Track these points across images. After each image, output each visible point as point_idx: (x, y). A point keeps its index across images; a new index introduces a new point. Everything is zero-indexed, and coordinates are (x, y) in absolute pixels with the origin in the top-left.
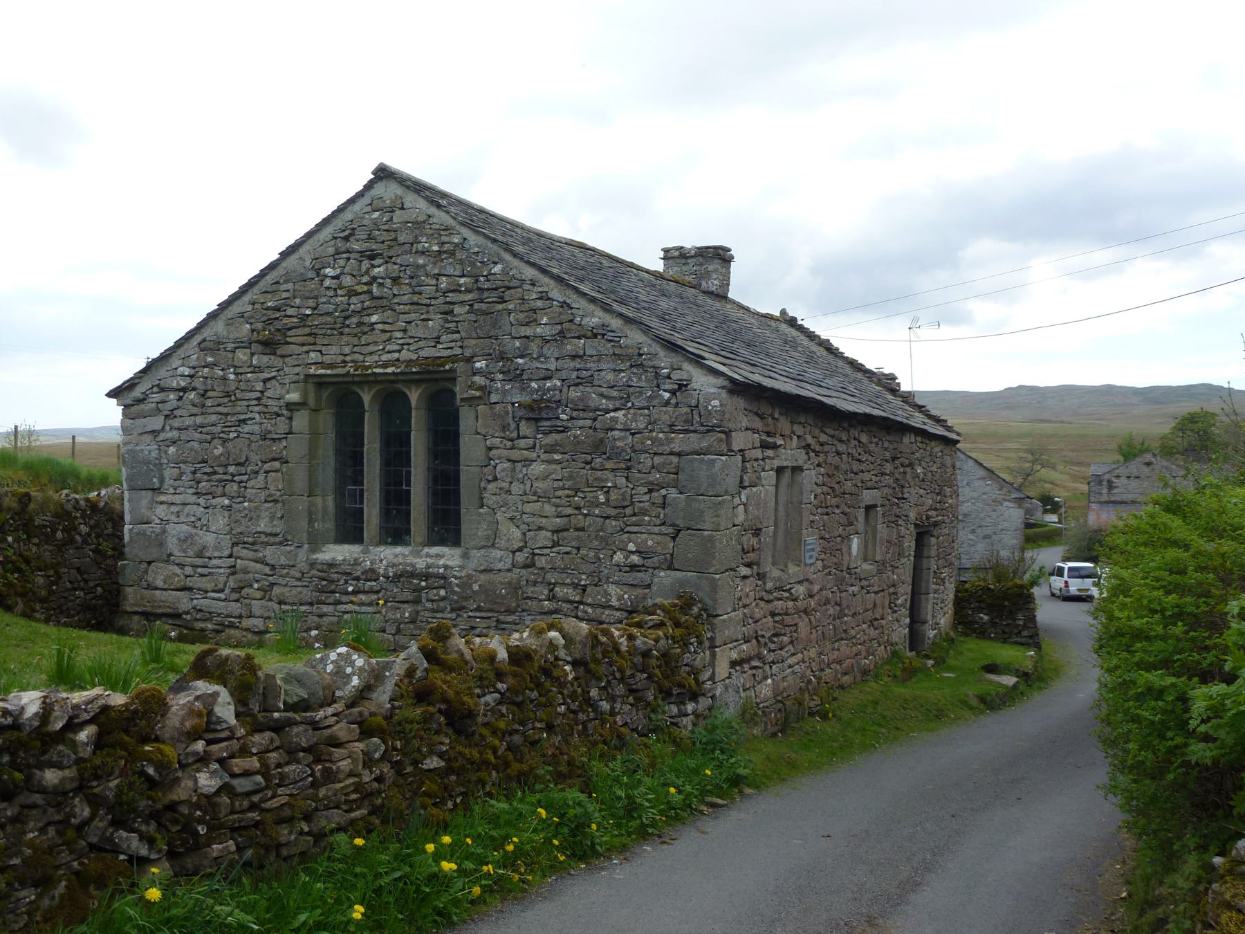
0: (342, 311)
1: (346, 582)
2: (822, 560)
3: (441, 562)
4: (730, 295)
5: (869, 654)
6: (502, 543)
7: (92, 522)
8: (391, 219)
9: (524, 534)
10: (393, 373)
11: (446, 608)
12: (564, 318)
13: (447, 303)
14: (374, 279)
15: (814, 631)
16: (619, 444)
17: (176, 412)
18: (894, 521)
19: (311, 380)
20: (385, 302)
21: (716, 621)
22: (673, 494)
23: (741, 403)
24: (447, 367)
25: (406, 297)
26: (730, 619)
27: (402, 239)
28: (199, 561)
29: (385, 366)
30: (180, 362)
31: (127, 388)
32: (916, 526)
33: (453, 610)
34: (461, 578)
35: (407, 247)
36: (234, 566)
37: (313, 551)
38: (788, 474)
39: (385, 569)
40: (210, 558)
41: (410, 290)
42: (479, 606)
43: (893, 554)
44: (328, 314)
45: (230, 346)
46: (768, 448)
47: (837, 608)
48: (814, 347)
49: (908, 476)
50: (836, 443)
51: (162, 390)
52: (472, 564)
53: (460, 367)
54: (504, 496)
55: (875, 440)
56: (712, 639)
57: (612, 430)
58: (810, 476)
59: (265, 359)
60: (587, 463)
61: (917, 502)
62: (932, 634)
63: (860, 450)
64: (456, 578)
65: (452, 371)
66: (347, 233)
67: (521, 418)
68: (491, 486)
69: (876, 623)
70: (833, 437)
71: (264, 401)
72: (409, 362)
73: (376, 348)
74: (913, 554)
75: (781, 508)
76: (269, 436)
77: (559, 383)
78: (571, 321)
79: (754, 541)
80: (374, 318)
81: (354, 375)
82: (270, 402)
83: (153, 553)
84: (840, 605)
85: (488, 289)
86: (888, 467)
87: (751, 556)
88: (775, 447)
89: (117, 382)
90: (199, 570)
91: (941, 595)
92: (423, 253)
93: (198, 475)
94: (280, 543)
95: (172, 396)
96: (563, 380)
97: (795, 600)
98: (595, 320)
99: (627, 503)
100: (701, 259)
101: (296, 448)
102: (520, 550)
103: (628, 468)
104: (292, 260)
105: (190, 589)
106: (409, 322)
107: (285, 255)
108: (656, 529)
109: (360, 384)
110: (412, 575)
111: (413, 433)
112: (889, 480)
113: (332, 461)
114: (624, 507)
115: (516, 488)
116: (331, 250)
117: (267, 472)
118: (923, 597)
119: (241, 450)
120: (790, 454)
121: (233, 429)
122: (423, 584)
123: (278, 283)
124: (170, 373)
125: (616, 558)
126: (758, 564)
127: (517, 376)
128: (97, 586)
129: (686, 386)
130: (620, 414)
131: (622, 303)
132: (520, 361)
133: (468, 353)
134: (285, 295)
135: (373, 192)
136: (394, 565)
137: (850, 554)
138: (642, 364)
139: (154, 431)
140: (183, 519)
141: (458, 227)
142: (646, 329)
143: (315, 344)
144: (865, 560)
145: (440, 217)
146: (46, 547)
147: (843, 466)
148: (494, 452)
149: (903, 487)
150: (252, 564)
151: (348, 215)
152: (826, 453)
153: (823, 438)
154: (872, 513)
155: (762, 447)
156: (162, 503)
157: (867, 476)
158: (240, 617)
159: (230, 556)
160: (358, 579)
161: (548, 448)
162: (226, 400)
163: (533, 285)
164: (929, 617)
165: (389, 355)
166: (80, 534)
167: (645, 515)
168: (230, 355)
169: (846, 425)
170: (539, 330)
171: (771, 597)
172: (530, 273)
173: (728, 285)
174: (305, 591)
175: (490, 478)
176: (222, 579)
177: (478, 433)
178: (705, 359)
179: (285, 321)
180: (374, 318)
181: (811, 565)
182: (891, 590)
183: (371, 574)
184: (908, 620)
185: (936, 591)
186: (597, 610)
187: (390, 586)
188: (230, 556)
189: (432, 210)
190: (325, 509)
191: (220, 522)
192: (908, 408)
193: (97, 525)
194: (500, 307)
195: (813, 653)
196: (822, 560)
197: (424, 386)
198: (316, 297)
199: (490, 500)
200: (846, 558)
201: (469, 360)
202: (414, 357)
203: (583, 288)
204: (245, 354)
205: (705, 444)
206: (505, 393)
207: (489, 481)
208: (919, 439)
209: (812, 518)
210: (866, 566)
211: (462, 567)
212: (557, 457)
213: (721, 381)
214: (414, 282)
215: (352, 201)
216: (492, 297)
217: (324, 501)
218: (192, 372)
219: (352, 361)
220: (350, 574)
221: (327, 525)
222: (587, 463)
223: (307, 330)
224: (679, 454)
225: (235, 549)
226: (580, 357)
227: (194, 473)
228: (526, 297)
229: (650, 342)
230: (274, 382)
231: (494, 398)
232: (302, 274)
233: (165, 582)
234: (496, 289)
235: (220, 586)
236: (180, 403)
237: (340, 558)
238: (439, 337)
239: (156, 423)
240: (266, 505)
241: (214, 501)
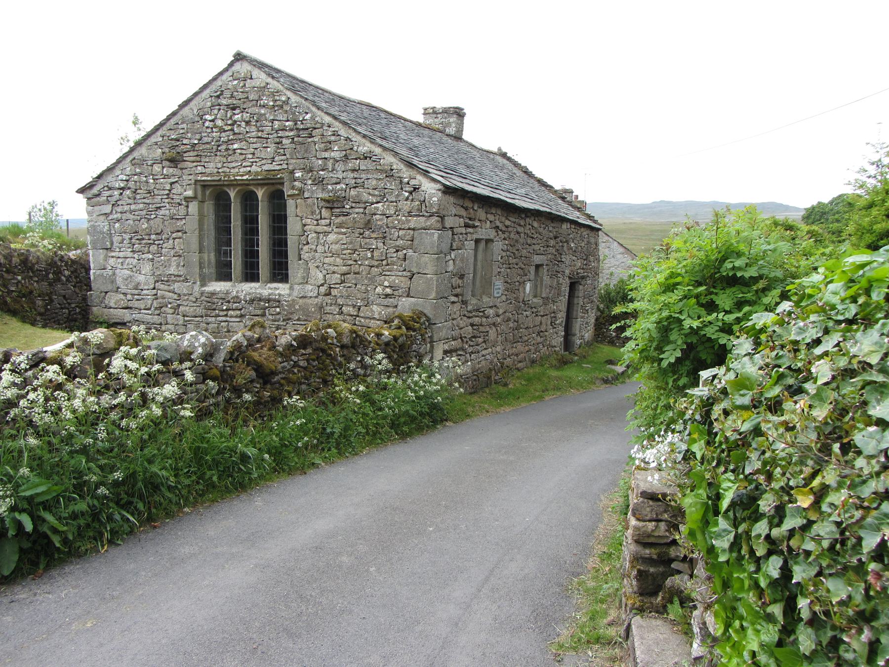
0: (216, 141)
1: (222, 304)
2: (506, 295)
3: (277, 292)
4: (463, 137)
5: (536, 351)
6: (311, 281)
7: (72, 269)
8: (245, 85)
9: (325, 276)
10: (247, 180)
11: (280, 319)
12: (347, 147)
13: (278, 137)
14: (235, 122)
15: (500, 336)
16: (379, 223)
17: (118, 203)
18: (554, 275)
19: (198, 183)
20: (241, 137)
21: (434, 327)
22: (410, 252)
23: (451, 199)
24: (279, 176)
26: (444, 326)
27: (251, 98)
28: (136, 292)
29: (242, 176)
30: (120, 172)
31: (88, 188)
32: (570, 278)
33: (284, 320)
34: (288, 301)
35: (254, 102)
36: (156, 295)
37: (203, 285)
38: (482, 245)
39: (245, 296)
40: (142, 290)
41: (256, 129)
42: (299, 318)
43: (554, 293)
44: (207, 143)
45: (150, 163)
46: (470, 227)
47: (516, 323)
48: (515, 170)
49: (565, 249)
50: (516, 226)
51: (110, 189)
52: (295, 293)
54: (313, 253)
55: (543, 226)
56: (431, 337)
57: (375, 215)
58: (498, 246)
59: (171, 170)
60: (361, 234)
61: (571, 264)
62: (578, 342)
63: (533, 231)
64: (286, 301)
65: (281, 178)
66: (218, 93)
67: (322, 207)
68: (306, 248)
69: (541, 334)
70: (514, 222)
71: (171, 196)
72: (257, 173)
73: (237, 164)
74: (567, 294)
75: (479, 264)
76: (175, 217)
77: (344, 187)
78: (351, 149)
79: (460, 281)
80: (235, 146)
82: (175, 197)
83: (110, 287)
84: (517, 322)
85: (303, 129)
86: (552, 243)
87: (458, 290)
88: (474, 227)
89: (82, 184)
90: (136, 297)
91: (586, 320)
92: (264, 106)
93: (133, 241)
94: (183, 281)
95: (116, 193)
96: (347, 185)
97: (487, 317)
101: (191, 224)
102: (322, 285)
103: (385, 237)
104: (186, 110)
105: (131, 308)
106: (256, 149)
107: (182, 106)
108: (400, 274)
109: (228, 186)
110: (260, 300)
112: (552, 250)
113: (213, 233)
114: (382, 260)
115: (320, 248)
116: (209, 104)
117: (174, 239)
119: (158, 225)
120: (485, 231)
121: (153, 213)
122: (267, 305)
123: (177, 124)
124: (114, 179)
125: (377, 290)
126: (462, 295)
127: (320, 182)
128: (77, 306)
129: (418, 188)
130: (380, 205)
131: (385, 139)
132: (321, 173)
133: (291, 167)
134: (182, 131)
135: (234, 68)
136: (250, 294)
137: (524, 293)
138: (392, 176)
139: (106, 214)
140: (125, 267)
141: (284, 91)
142: (396, 154)
143: (200, 161)
144: (535, 296)
145: (274, 84)
147: (521, 240)
148: (307, 227)
149: (561, 254)
150: (167, 293)
151: (219, 83)
152: (510, 232)
153: (508, 223)
154: (541, 269)
155: (465, 226)
156: (113, 257)
157: (537, 247)
158: (161, 324)
159: (154, 289)
160: (229, 302)
161: (338, 225)
162: (149, 195)
164: (577, 332)
165: (245, 169)
166: (65, 276)
167: (394, 265)
168: (150, 168)
169: (523, 216)
170: (333, 154)
171: (471, 315)
172: (328, 119)
173: (462, 131)
174: (198, 309)
175: (305, 243)
176: (150, 302)
177: (297, 216)
178: (429, 172)
179: (182, 147)
180: (235, 146)
181: (498, 297)
182: (553, 315)
183: (237, 299)
184: (563, 333)
185: (582, 317)
186: (367, 320)
187: (247, 306)
188: (154, 289)
189: (270, 80)
191: (147, 268)
192: (571, 208)
193: (76, 271)
194: (310, 140)
195: (499, 349)
196: (506, 295)
197: (265, 188)
198: (200, 133)
199: (305, 256)
200: (522, 294)
201: (292, 172)
202: (259, 170)
203: (359, 129)
204: (159, 167)
205: (428, 223)
206: (312, 192)
207: (304, 245)
208: (573, 226)
209: (499, 270)
210: (535, 300)
211: (289, 295)
212: (344, 230)
213: (438, 186)
214: (258, 124)
215: (221, 74)
216: (304, 134)
217: (209, 256)
218: (128, 178)
219: (223, 172)
220: (224, 299)
221: (210, 270)
222: (361, 234)
223: (195, 153)
224: (414, 229)
225: (157, 284)
226: (357, 171)
227: (131, 239)
229: (397, 162)
230: (177, 184)
231: (306, 195)
233: (116, 304)
234: (307, 129)
235: (149, 306)
236: (121, 197)
237: (219, 290)
238: (274, 158)
239: (107, 209)
240: (174, 258)
241: (143, 256)
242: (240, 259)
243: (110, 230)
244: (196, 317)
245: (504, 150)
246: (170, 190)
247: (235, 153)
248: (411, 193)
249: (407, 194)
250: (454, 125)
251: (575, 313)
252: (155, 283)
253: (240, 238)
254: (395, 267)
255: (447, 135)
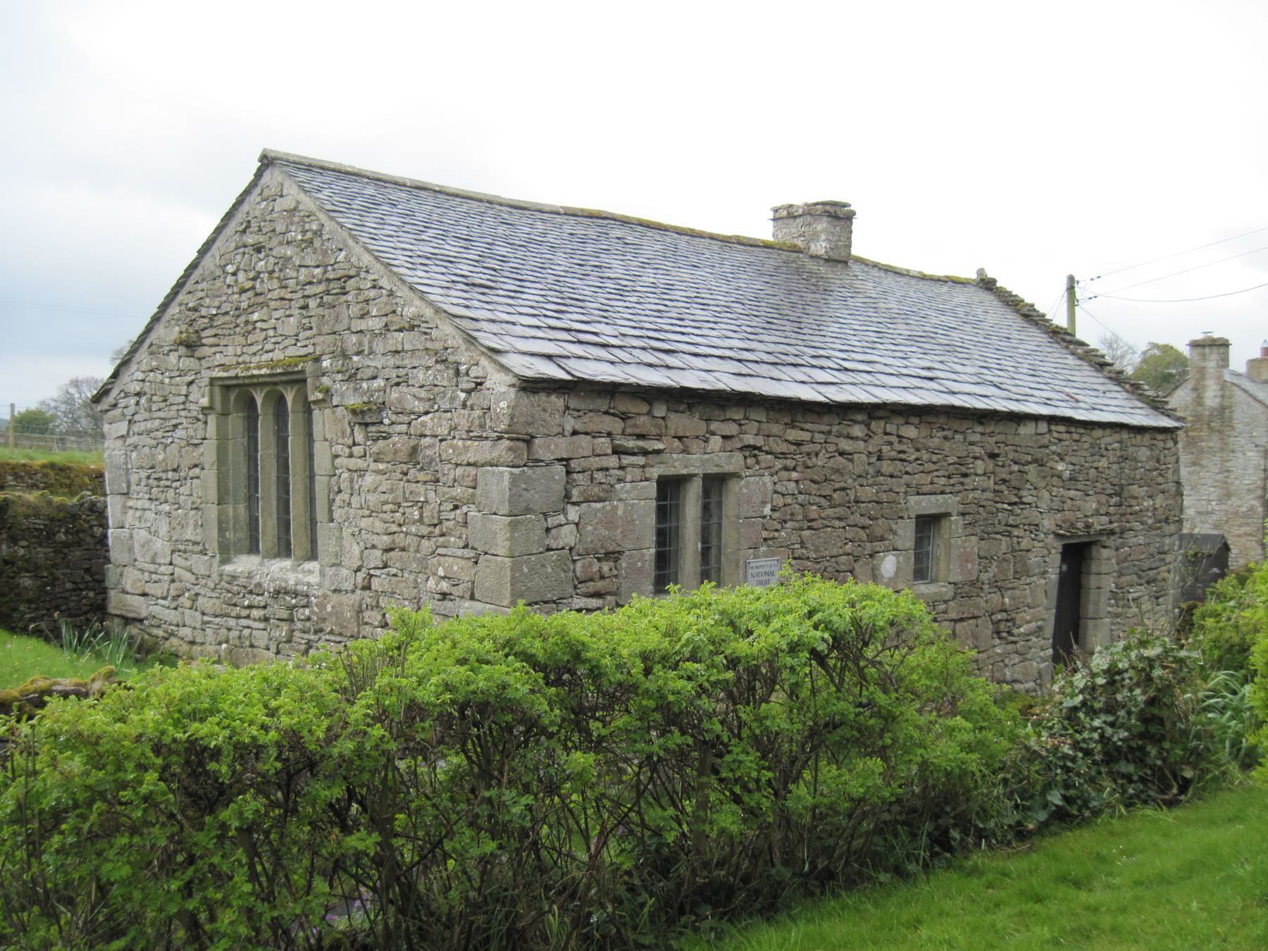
16: (429, 452)
25: (276, 292)
28: (152, 567)
53: (309, 367)
54: (346, 508)
65: (302, 372)
78: (394, 312)
80: (256, 316)
81: (244, 377)
96: (387, 379)
98: (413, 309)
99: (436, 522)
100: (809, 218)
101: (208, 453)
109: (254, 385)
111: (290, 439)
115: (355, 501)
117: (192, 478)
118: (1090, 623)
129: (481, 384)
146: (39, 549)
148: (338, 461)
153: (793, 435)
163: (367, 272)
167: (451, 535)
180: (256, 316)
183: (257, 590)
189: (302, 196)
190: (236, 518)
199: (337, 514)
201: (317, 360)
211: (320, 585)
217: (235, 510)
228: (362, 287)
232: (212, 272)
234: (339, 279)
235: (165, 594)
237: (239, 570)
242: (275, 516)
243: (126, 463)
244: (216, 616)
245: (990, 275)
246: (186, 396)
247: (255, 328)
248: (469, 392)
249: (463, 395)
250: (823, 237)
251: (1091, 607)
252: (172, 554)
253: (274, 478)
254: (452, 539)
255: (812, 257)
